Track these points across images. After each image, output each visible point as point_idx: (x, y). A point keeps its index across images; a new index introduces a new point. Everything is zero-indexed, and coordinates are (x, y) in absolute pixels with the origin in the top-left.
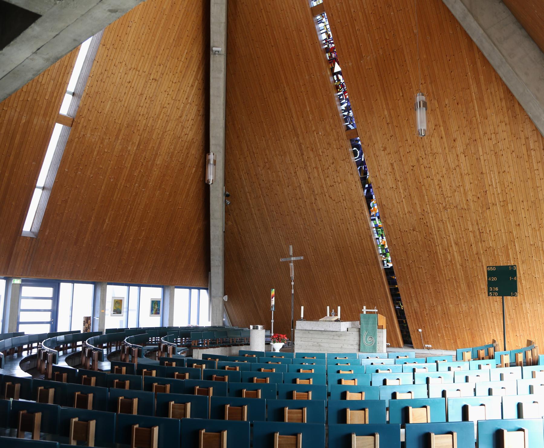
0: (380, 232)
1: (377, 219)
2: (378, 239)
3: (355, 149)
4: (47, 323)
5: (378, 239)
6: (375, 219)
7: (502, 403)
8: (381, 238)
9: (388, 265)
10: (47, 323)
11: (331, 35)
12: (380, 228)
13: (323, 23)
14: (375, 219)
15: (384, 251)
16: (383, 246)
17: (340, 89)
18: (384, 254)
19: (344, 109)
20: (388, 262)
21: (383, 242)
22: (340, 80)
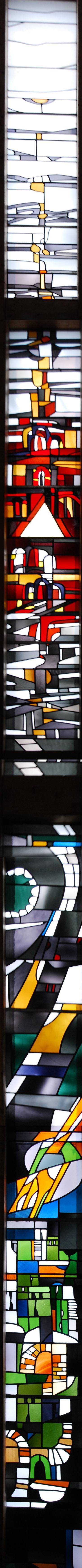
0: (44, 1307)
1: (41, 1232)
2: (18, 1339)
3: (19, 871)
4: (73, 273)
5: (18, 1339)
6: (28, 1234)
7: (18, 113)
8: (34, 1336)
9: (34, 1496)
10: (73, 273)
11: (71, 893)
12: (43, 1282)
13: (38, 358)
14: (28, 1234)
15: (35, 1412)
16: (38, 1379)
17: (27, 602)
18: (25, 1428)
19: (20, 674)
20: (40, 1473)
21: (44, 1360)
22: (41, 571)
